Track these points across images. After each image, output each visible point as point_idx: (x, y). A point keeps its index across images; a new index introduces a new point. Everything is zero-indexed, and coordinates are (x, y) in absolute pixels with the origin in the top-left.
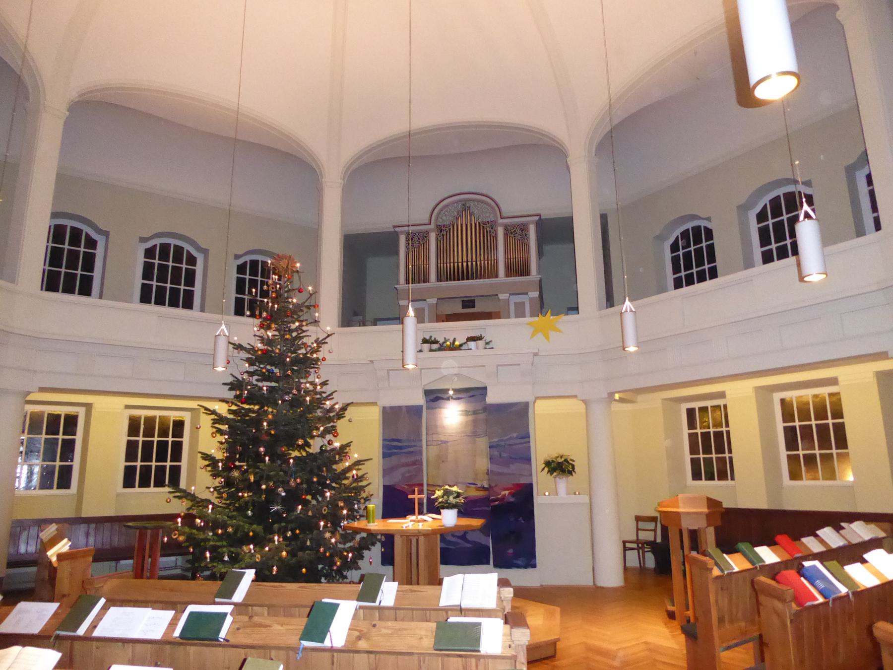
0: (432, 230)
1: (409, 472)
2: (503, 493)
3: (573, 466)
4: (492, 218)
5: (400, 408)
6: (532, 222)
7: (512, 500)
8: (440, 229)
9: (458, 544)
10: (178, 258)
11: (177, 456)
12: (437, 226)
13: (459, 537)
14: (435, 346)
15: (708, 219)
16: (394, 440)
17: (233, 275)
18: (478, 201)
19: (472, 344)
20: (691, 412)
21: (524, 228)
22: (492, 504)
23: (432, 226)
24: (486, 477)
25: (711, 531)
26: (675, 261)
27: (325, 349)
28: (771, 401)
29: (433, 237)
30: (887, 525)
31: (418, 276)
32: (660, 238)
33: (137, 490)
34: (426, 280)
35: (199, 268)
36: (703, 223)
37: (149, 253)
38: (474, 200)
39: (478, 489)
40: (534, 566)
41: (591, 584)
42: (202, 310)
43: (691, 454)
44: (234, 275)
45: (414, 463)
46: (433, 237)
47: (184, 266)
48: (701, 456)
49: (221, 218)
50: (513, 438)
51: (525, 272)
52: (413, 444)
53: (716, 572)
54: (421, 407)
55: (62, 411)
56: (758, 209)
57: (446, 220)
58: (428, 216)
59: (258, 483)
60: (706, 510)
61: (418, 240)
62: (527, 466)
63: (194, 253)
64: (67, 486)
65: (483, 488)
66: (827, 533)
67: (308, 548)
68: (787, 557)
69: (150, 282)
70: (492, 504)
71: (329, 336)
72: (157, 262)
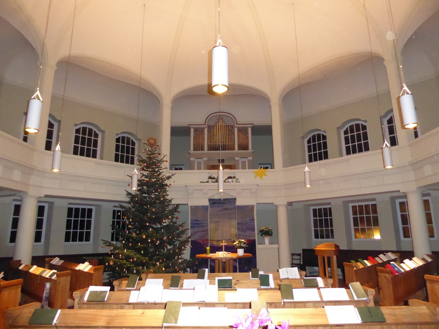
0: (206, 127)
3: (272, 232)
4: (232, 124)
5: (198, 207)
8: (210, 127)
10: (90, 134)
11: (89, 227)
12: (208, 126)
14: (214, 180)
15: (325, 132)
16: (195, 221)
17: (114, 143)
18: (226, 116)
19: (230, 180)
20: (315, 210)
21: (246, 129)
23: (206, 126)
25: (335, 257)
26: (309, 147)
27: (171, 180)
28: (348, 208)
29: (206, 130)
30: (398, 254)
31: (199, 147)
32: (303, 138)
33: (78, 243)
34: (203, 149)
35: (99, 139)
36: (321, 133)
38: (224, 115)
42: (101, 158)
44: (74, 134)
45: (205, 231)
46: (206, 130)
47: (93, 138)
48: (319, 229)
49: (112, 118)
51: (246, 148)
53: (355, 269)
54: (208, 206)
55: (87, 207)
56: (345, 129)
57: (212, 123)
58: (204, 121)
59: (146, 239)
60: (334, 249)
61: (199, 131)
62: (253, 232)
63: (97, 132)
64: (89, 241)
66: (381, 256)
67: (171, 267)
68: (373, 264)
69: (78, 145)
71: (173, 175)
72: (81, 135)
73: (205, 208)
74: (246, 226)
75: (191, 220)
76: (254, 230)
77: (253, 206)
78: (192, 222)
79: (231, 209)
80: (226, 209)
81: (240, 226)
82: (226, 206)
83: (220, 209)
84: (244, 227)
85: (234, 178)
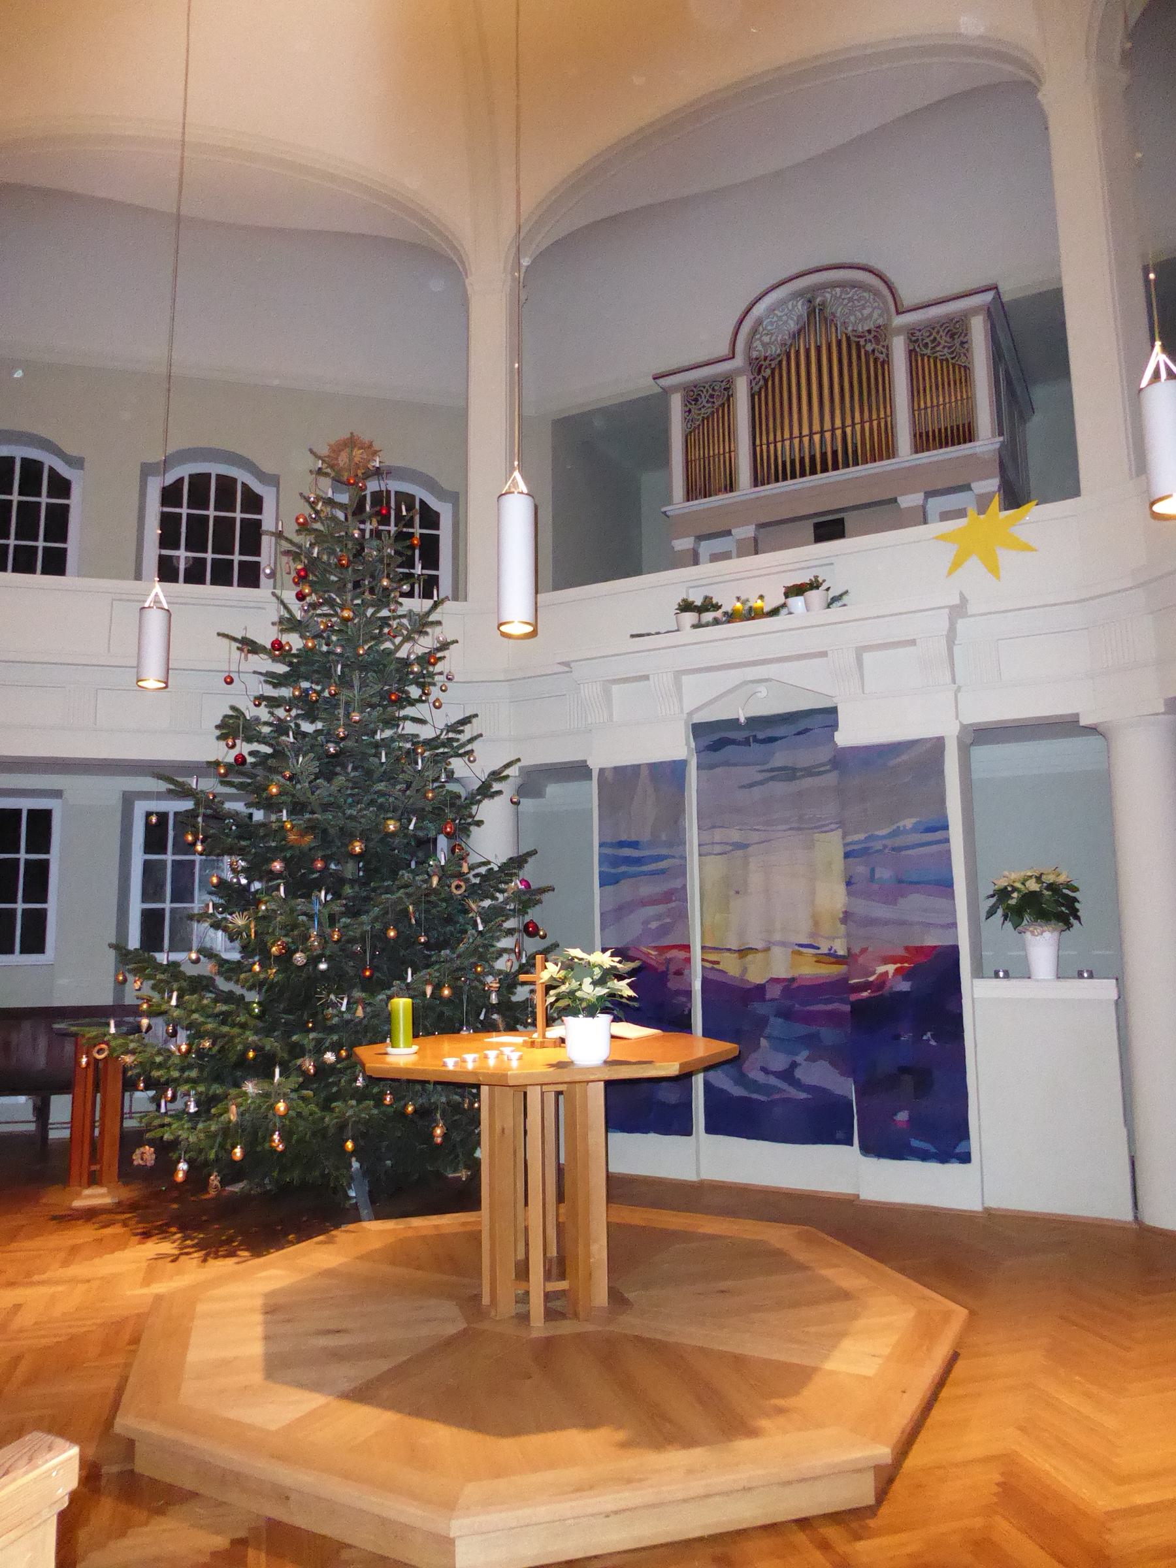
1: (658, 917)
2: (881, 969)
5: (636, 768)
6: (975, 311)
7: (905, 986)
9: (780, 1090)
13: (778, 1075)
14: (708, 616)
16: (622, 844)
18: (841, 285)
19: (797, 603)
21: (956, 329)
22: (854, 997)
23: (739, 362)
24: (842, 928)
35: (445, 533)
37: (170, 495)
39: (821, 959)
40: (965, 1158)
41: (1129, 1217)
43: (30, 811)
47: (238, 515)
50: (905, 832)
52: (664, 851)
61: (708, 401)
62: (940, 903)
65: (833, 957)
70: (854, 997)
73: (669, 775)
74: (900, 865)
75: (601, 845)
76: (946, 885)
77: (938, 744)
78: (609, 851)
79: (810, 772)
80: (790, 773)
81: (861, 869)
82: (780, 758)
83: (752, 773)
84: (884, 874)
85: (814, 585)
